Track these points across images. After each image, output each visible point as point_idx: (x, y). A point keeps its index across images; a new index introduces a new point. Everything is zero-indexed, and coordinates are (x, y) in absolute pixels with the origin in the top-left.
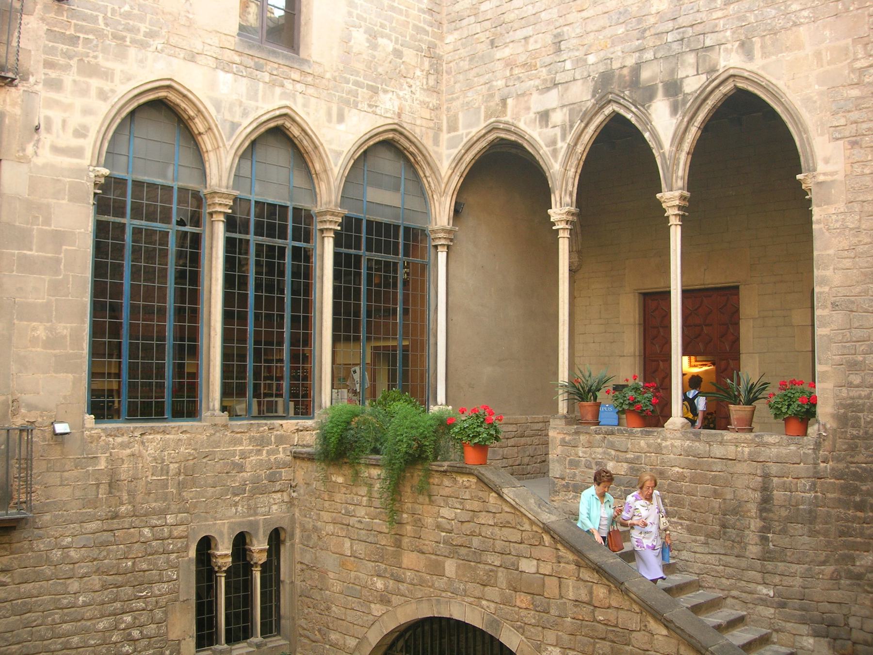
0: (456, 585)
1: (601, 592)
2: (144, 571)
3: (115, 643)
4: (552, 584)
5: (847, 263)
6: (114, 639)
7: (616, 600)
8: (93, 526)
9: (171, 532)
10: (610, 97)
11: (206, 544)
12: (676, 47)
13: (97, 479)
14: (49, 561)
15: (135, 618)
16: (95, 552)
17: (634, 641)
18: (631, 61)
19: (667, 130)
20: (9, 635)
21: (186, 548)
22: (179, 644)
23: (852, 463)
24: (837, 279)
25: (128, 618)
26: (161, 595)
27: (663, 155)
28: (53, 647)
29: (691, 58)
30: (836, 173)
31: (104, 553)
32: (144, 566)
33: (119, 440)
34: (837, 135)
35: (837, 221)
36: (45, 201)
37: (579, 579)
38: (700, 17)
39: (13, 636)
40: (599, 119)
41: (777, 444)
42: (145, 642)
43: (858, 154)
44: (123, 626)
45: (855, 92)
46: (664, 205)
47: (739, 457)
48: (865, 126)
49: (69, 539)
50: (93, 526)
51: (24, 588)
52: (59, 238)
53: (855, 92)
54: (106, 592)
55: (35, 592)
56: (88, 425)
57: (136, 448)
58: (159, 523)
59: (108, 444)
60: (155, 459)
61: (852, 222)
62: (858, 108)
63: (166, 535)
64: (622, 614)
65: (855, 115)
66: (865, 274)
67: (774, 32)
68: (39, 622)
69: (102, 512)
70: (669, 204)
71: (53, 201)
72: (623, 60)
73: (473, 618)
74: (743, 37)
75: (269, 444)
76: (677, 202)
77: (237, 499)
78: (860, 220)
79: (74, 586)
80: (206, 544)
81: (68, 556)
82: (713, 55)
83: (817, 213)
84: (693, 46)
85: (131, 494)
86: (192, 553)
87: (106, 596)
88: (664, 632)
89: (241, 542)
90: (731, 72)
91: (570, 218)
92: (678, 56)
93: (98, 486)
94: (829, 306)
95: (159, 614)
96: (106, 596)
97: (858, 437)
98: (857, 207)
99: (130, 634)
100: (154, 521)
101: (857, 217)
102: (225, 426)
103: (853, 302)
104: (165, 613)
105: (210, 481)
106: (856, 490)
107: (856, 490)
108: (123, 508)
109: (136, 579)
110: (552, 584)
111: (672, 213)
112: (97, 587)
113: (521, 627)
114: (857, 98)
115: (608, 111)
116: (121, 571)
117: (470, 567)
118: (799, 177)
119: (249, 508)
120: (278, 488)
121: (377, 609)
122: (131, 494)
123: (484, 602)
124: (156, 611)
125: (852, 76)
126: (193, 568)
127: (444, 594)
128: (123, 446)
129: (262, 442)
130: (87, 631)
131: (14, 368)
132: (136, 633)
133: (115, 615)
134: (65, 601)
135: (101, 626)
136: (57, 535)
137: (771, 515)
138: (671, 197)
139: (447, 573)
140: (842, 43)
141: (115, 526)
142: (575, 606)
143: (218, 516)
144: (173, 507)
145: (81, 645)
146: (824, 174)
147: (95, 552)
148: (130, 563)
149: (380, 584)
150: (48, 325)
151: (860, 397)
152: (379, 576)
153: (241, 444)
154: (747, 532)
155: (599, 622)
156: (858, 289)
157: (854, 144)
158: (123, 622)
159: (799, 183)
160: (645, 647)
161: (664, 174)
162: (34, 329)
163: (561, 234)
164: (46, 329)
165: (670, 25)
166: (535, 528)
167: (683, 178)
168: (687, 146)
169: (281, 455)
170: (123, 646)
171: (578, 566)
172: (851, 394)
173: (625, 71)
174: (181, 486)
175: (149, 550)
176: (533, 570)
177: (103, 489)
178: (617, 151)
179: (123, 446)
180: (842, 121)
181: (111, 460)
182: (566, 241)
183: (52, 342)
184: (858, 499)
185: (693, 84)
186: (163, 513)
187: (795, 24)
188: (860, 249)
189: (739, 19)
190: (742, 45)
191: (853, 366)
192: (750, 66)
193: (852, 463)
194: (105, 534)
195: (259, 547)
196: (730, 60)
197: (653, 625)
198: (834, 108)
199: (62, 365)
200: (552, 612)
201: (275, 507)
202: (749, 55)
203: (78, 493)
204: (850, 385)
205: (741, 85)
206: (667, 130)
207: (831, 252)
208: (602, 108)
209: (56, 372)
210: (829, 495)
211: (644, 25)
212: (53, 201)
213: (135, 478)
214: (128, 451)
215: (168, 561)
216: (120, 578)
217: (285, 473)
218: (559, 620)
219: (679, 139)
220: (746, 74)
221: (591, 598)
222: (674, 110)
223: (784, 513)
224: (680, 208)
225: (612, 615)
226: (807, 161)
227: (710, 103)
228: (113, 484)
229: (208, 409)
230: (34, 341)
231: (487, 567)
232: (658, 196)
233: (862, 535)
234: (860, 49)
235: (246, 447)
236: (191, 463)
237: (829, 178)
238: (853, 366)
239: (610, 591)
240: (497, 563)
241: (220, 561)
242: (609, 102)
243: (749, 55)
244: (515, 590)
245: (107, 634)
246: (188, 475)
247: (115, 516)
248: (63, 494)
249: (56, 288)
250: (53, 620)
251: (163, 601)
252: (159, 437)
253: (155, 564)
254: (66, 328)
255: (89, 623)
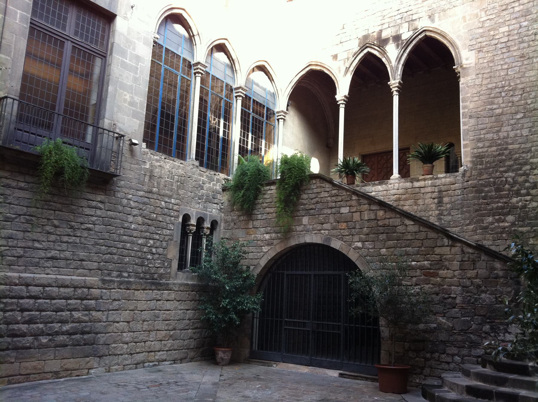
0: (308, 227)
1: (381, 213)
2: (161, 222)
3: (145, 252)
4: (356, 216)
5: (476, 99)
6: (145, 250)
7: (388, 215)
8: (141, 193)
9: (173, 206)
10: (367, 45)
11: (186, 218)
12: (399, 21)
13: (145, 172)
14: (121, 204)
15: (154, 243)
16: (141, 206)
17: (398, 231)
18: (377, 29)
19: (393, 58)
20: (100, 234)
21: (178, 217)
22: (171, 262)
23: (480, 180)
24: (472, 106)
25: (151, 242)
26: (166, 235)
27: (391, 67)
28: (118, 246)
29: (406, 25)
30: (471, 63)
31: (144, 208)
32: (161, 219)
33: (156, 157)
34: (472, 49)
35: (471, 83)
36: (134, 40)
37: (370, 210)
38: (410, 8)
39: (102, 235)
40: (362, 55)
41: (444, 178)
42: (157, 256)
43: (481, 55)
44: (149, 245)
45: (481, 31)
46: (391, 87)
47: (426, 186)
48: (484, 43)
49: (131, 196)
50: (141, 193)
51: (109, 213)
52: (138, 58)
53: (481, 31)
54: (144, 226)
55: (113, 216)
56: (143, 147)
57: (162, 163)
58: (168, 201)
59: (151, 157)
60: (169, 171)
61: (478, 82)
62: (482, 37)
63: (171, 207)
64: (391, 220)
65: (480, 40)
66: (484, 102)
67: (444, 10)
68: (113, 231)
69: (145, 188)
70: (393, 86)
71: (137, 42)
72: (373, 29)
73: (316, 239)
74: (430, 14)
75: (213, 181)
76: (398, 85)
77: (200, 201)
78: (482, 81)
79: (131, 219)
80: (186, 218)
81: (130, 204)
82: (416, 23)
83: (462, 81)
84: (407, 20)
85: (158, 184)
86: (180, 220)
87: (144, 228)
88: (413, 223)
89: (201, 221)
90: (424, 29)
91: (346, 99)
92: (400, 25)
93: (145, 175)
94: (468, 117)
95: (164, 244)
96: (144, 228)
97: (482, 169)
98: (480, 76)
99: (151, 250)
100: (167, 200)
101: (481, 80)
102: (197, 167)
103: (479, 114)
104: (167, 244)
105: (190, 189)
106: (482, 191)
107: (482, 191)
108: (154, 189)
109: (156, 224)
110: (356, 216)
111: (394, 90)
112: (140, 223)
113: (341, 238)
114: (481, 33)
115: (365, 51)
116: (151, 218)
117: (316, 218)
118: (454, 67)
119: (204, 207)
120: (216, 202)
121: (265, 249)
122: (158, 184)
123: (322, 231)
124: (163, 242)
125: (479, 24)
126: (180, 227)
127: (301, 233)
128: (157, 161)
129: (211, 180)
130: (133, 243)
131: (115, 109)
132: (154, 250)
133: (146, 239)
134: (126, 225)
135: (140, 242)
136: (126, 192)
137: (442, 208)
138: (394, 82)
139: (304, 223)
140: (475, 12)
141: (150, 197)
142: (368, 222)
143: (192, 206)
144: (174, 196)
145: (130, 248)
146: (466, 65)
147: (141, 206)
148: (155, 216)
149: (267, 236)
150: (131, 95)
151: (483, 152)
152: (266, 233)
153: (203, 177)
154: (430, 217)
155: (380, 226)
156: (481, 108)
157: (479, 51)
158: (149, 243)
159: (454, 70)
160: (404, 231)
161: (392, 74)
162: (125, 95)
163: (341, 106)
164: (130, 97)
165: (396, 13)
166: (348, 193)
167: (400, 75)
168: (402, 62)
169: (218, 188)
170: (148, 255)
171: (370, 205)
172: (479, 151)
173: (375, 34)
174: (179, 187)
175: (163, 212)
176: (347, 211)
177: (147, 179)
178: (369, 70)
179: (157, 161)
180: (475, 43)
181: (151, 166)
182: (343, 109)
183: (132, 104)
184: (483, 194)
185: (406, 35)
186: (170, 197)
187: (454, 7)
188: (482, 92)
189: (428, 7)
190: (430, 17)
191: (479, 140)
192: (433, 25)
193: (480, 180)
194: (146, 199)
195: (207, 225)
196: (424, 24)
197: (408, 222)
198: (471, 38)
199: (135, 115)
200: (357, 227)
201: (214, 210)
202: (433, 21)
203: (137, 176)
204: (478, 148)
205: (428, 34)
206: (393, 58)
207: (469, 95)
208: (362, 51)
209: (132, 117)
210: (470, 195)
211: (384, 14)
212: (137, 42)
213: (160, 177)
214: (159, 164)
215: (170, 220)
216: (150, 222)
217: (219, 196)
218: (360, 230)
219: (399, 59)
220: (431, 29)
221: (376, 217)
222: (398, 46)
223: (449, 206)
224: (398, 87)
225: (386, 222)
226: (458, 61)
227: (414, 43)
228: (151, 177)
229: (190, 158)
230: (125, 100)
231: (324, 216)
232: (389, 83)
233: (486, 210)
234: (483, 14)
235: (204, 178)
236: (183, 178)
237: (468, 66)
238: (479, 140)
239: (385, 212)
240: (329, 212)
241: (191, 227)
242: (367, 47)
243: (433, 21)
244: (338, 222)
245: (142, 247)
246: (182, 184)
247: (151, 192)
248: (131, 175)
249: (136, 80)
250: (120, 232)
251: (167, 238)
252: (171, 162)
253: (165, 220)
254: (138, 99)
255: (135, 239)
